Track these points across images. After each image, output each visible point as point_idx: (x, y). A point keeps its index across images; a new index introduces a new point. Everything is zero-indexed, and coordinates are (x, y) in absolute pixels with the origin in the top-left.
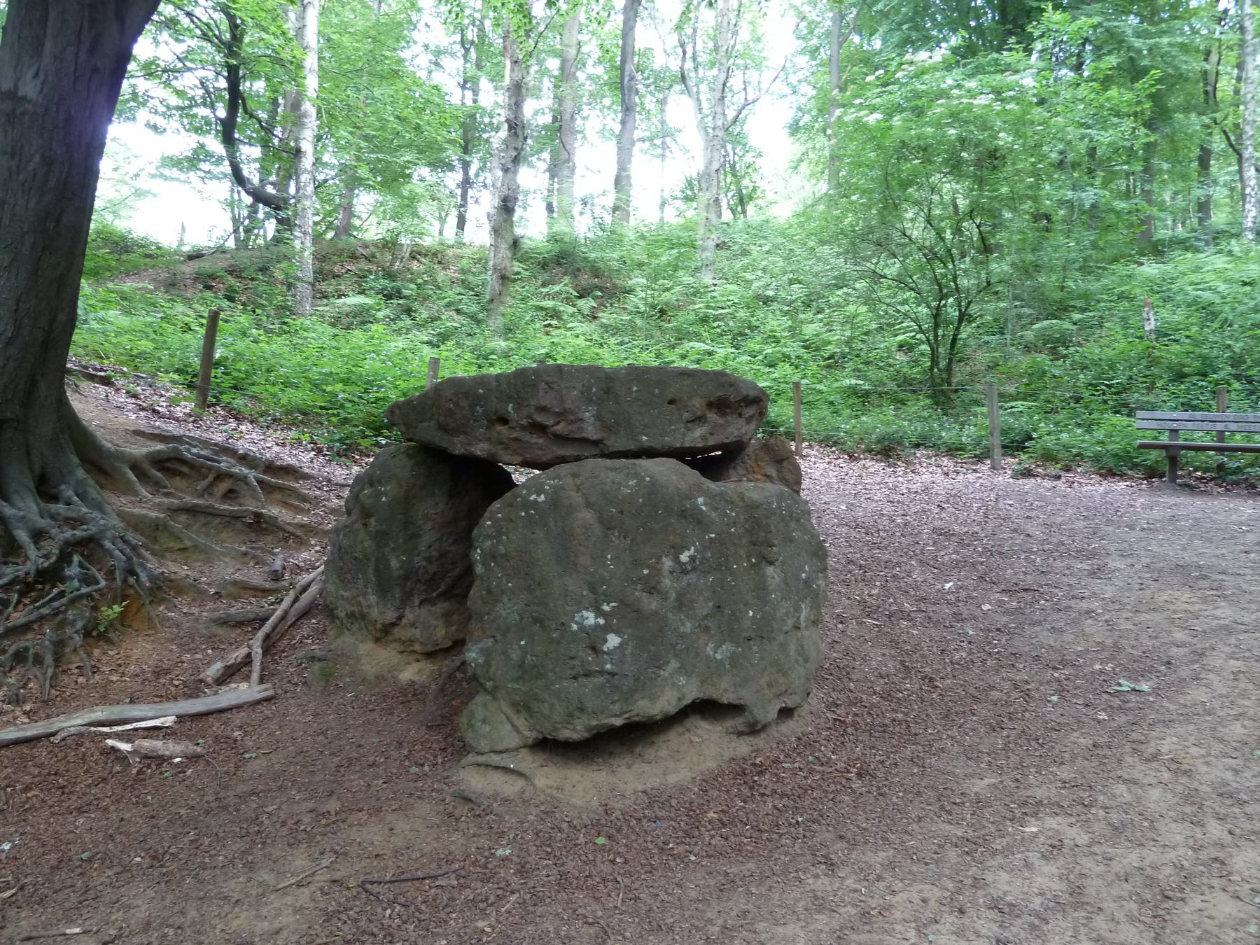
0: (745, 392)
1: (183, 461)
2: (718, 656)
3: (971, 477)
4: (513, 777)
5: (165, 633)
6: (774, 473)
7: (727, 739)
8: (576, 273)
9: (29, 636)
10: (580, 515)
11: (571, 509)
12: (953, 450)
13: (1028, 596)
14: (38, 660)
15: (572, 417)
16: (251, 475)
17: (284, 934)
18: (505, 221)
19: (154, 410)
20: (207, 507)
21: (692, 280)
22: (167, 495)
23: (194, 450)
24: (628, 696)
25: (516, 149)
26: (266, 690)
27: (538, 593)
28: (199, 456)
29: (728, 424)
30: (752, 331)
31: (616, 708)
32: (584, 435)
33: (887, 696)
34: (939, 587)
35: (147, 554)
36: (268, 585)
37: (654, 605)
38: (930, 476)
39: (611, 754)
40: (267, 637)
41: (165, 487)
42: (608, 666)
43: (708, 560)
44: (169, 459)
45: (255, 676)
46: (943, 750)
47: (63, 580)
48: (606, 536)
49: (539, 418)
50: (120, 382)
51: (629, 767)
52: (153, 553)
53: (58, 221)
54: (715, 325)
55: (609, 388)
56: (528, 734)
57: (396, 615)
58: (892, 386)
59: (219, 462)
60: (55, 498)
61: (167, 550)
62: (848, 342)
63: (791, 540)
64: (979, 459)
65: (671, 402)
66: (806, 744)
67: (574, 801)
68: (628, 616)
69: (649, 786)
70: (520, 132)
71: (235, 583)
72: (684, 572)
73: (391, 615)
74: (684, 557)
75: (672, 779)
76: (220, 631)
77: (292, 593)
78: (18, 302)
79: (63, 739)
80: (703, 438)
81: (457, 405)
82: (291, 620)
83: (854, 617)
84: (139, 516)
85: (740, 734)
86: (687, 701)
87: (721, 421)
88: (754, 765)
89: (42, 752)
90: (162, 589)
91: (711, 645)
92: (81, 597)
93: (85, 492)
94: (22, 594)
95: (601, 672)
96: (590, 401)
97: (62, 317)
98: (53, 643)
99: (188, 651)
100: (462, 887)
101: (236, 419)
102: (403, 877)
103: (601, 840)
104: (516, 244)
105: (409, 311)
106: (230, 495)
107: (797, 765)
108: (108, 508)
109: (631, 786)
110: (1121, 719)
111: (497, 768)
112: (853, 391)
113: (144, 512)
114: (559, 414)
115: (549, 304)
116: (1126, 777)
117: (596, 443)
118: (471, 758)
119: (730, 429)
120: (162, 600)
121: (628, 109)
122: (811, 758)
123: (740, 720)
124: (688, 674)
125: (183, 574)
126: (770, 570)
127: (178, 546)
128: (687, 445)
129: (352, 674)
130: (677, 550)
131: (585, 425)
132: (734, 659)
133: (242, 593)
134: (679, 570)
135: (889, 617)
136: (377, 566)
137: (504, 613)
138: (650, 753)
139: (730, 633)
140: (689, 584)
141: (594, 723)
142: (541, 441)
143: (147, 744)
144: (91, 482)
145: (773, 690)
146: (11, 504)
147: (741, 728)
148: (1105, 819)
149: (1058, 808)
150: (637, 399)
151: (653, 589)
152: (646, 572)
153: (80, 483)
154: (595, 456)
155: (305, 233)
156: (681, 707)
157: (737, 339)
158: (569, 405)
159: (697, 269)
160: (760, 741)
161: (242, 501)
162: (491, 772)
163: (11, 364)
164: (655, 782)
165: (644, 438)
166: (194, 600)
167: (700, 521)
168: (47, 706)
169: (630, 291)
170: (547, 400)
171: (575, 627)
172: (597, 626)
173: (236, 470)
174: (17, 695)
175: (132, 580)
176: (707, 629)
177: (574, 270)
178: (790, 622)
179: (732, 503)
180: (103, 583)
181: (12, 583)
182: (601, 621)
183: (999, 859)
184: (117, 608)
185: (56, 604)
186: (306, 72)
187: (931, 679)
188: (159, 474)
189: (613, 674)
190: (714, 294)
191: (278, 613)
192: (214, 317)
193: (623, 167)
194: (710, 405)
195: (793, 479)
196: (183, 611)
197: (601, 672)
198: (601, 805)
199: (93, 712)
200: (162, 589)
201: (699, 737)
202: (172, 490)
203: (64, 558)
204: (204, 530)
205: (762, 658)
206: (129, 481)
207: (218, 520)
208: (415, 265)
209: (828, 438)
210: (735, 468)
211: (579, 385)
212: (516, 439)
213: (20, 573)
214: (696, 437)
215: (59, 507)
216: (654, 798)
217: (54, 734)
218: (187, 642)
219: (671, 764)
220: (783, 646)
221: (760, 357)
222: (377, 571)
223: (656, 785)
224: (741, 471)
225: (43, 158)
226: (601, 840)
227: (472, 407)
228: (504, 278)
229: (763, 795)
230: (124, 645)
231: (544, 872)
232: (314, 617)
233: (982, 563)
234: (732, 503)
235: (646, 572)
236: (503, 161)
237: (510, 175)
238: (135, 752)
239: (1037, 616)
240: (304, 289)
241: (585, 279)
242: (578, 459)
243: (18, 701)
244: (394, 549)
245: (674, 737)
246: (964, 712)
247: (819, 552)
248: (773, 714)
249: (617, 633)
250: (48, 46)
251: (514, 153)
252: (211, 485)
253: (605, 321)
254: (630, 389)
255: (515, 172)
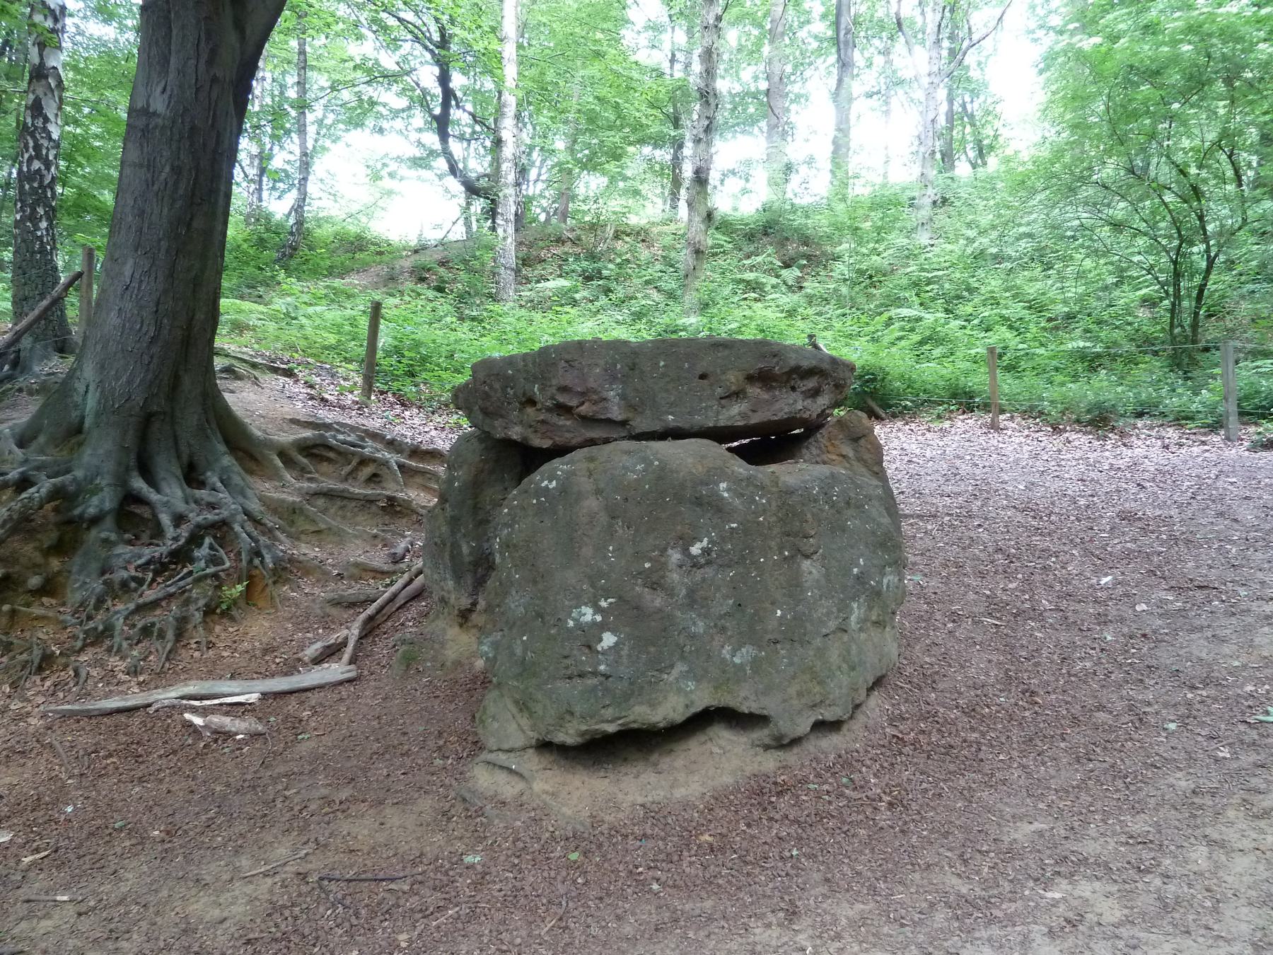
0: (793, 363)
1: (330, 448)
2: (737, 660)
3: (1196, 450)
4: (516, 778)
5: (284, 612)
6: (851, 454)
7: (752, 752)
8: (783, 242)
9: (158, 612)
10: (586, 503)
11: (580, 496)
12: (1181, 419)
13: (1200, 595)
14: (161, 635)
15: (595, 397)
16: (393, 458)
17: (226, 924)
18: (698, 193)
19: (323, 399)
20: (343, 491)
21: (906, 241)
22: (310, 480)
23: (341, 437)
24: (626, 698)
25: (708, 118)
26: (349, 671)
27: (540, 586)
28: (344, 442)
29: (775, 399)
30: (971, 294)
31: (608, 713)
32: (609, 416)
33: (970, 711)
34: (1094, 581)
35: (282, 537)
36: (386, 568)
37: (658, 602)
38: (1147, 449)
39: (625, 760)
40: (371, 618)
41: (310, 472)
42: (602, 667)
43: (728, 552)
44: (315, 446)
45: (346, 657)
46: (1004, 782)
47: (192, 560)
48: (611, 526)
49: (562, 399)
50: (301, 373)
51: (637, 777)
52: (289, 536)
53: (189, 226)
54: (928, 288)
55: (634, 364)
56: (531, 734)
57: (470, 601)
58: (1128, 347)
59: (363, 447)
60: (202, 485)
61: (302, 532)
62: (1080, 299)
63: (844, 529)
64: (1214, 427)
65: (703, 377)
66: (847, 762)
67: (564, 809)
68: (628, 613)
69: (650, 799)
70: (711, 100)
71: (357, 565)
72: (696, 566)
73: (465, 602)
74: (695, 550)
75: (679, 793)
76: (334, 612)
77: (406, 576)
78: (158, 304)
79: (157, 711)
80: (743, 415)
81: (491, 387)
82: (400, 601)
83: (972, 616)
84: (278, 500)
85: (767, 748)
86: (694, 710)
87: (766, 396)
88: (775, 783)
89: (136, 720)
90: (285, 570)
91: (728, 648)
92: (206, 577)
93: (229, 478)
94: (157, 573)
95: (595, 673)
96: (614, 379)
97: (200, 316)
98: (177, 620)
99: (301, 630)
100: (413, 893)
101: (403, 405)
102: (363, 876)
103: (574, 856)
104: (709, 216)
105: (607, 291)
106: (374, 478)
107: (826, 787)
108: (249, 493)
109: (630, 798)
110: (1248, 758)
111: (501, 767)
112: (1082, 355)
113: (284, 496)
114: (583, 394)
115: (750, 276)
116: (1215, 836)
117: (624, 423)
118: (485, 756)
119: (777, 406)
120: (287, 581)
121: (844, 65)
122: (845, 780)
123: (766, 731)
124: (698, 680)
125: (312, 555)
126: (806, 564)
127: (313, 529)
128: (722, 423)
129: (434, 659)
130: (685, 542)
131: (609, 405)
132: (756, 663)
133: (364, 575)
134: (689, 563)
135: (1016, 615)
136: (452, 552)
137: (513, 606)
138: (665, 763)
139: (750, 635)
140: (704, 580)
141: (584, 728)
142: (568, 423)
143: (216, 720)
144: (237, 468)
145: (804, 701)
146: (158, 491)
147: (767, 741)
148: (1158, 890)
149: (1103, 869)
150: (664, 375)
151: (656, 583)
152: (647, 565)
153: (225, 470)
154: (623, 438)
155: (507, 221)
156: (688, 715)
157: (950, 304)
158: (592, 383)
159: (914, 230)
160: (791, 757)
161: (384, 485)
162: (497, 771)
163: (155, 360)
164: (659, 795)
165: (671, 417)
166: (318, 581)
167: (718, 508)
168: (161, 677)
169: (836, 258)
170: (568, 379)
171: (571, 623)
172: (594, 623)
173: (379, 455)
174: (136, 667)
175: (257, 561)
176: (723, 630)
177: (782, 240)
178: (832, 625)
179: (763, 488)
180: (228, 564)
181: (148, 563)
182: (599, 618)
183: (995, 931)
184: (240, 588)
185: (182, 583)
186: (505, 62)
187: (1033, 693)
188: (305, 461)
189: (607, 677)
190: (928, 255)
191: (386, 595)
192: (376, 309)
193: (843, 129)
194: (750, 379)
195: (873, 459)
196: (310, 593)
197: (595, 673)
198: (592, 816)
199: (186, 685)
200: (285, 570)
201: (720, 748)
202: (316, 475)
203: (195, 539)
204: (340, 513)
205: (791, 664)
206: (276, 468)
207: (354, 504)
208: (619, 245)
209: (1032, 408)
210: (807, 448)
211: (602, 362)
212: (543, 422)
213: (157, 555)
214: (733, 414)
215: (203, 494)
216: (652, 813)
217: (149, 705)
218: (303, 622)
219: (681, 777)
220: (821, 652)
221: (976, 322)
222: (452, 557)
223: (657, 799)
224: (815, 451)
225: (173, 169)
226: (574, 856)
227: (504, 389)
228: (698, 252)
229: (771, 819)
230: (245, 623)
231: (498, 887)
232: (424, 599)
233: (1159, 554)
234: (763, 488)
235: (647, 565)
236: (695, 132)
237: (702, 146)
238: (205, 727)
239: (1203, 620)
240: (507, 276)
241: (791, 248)
242: (607, 441)
243: (135, 672)
244: (464, 536)
245: (695, 747)
246: (1052, 737)
247: (889, 546)
248: (804, 726)
249: (614, 632)
250: (173, 60)
251: (706, 123)
252: (355, 470)
253: (809, 291)
254: (657, 364)
255: (709, 144)
